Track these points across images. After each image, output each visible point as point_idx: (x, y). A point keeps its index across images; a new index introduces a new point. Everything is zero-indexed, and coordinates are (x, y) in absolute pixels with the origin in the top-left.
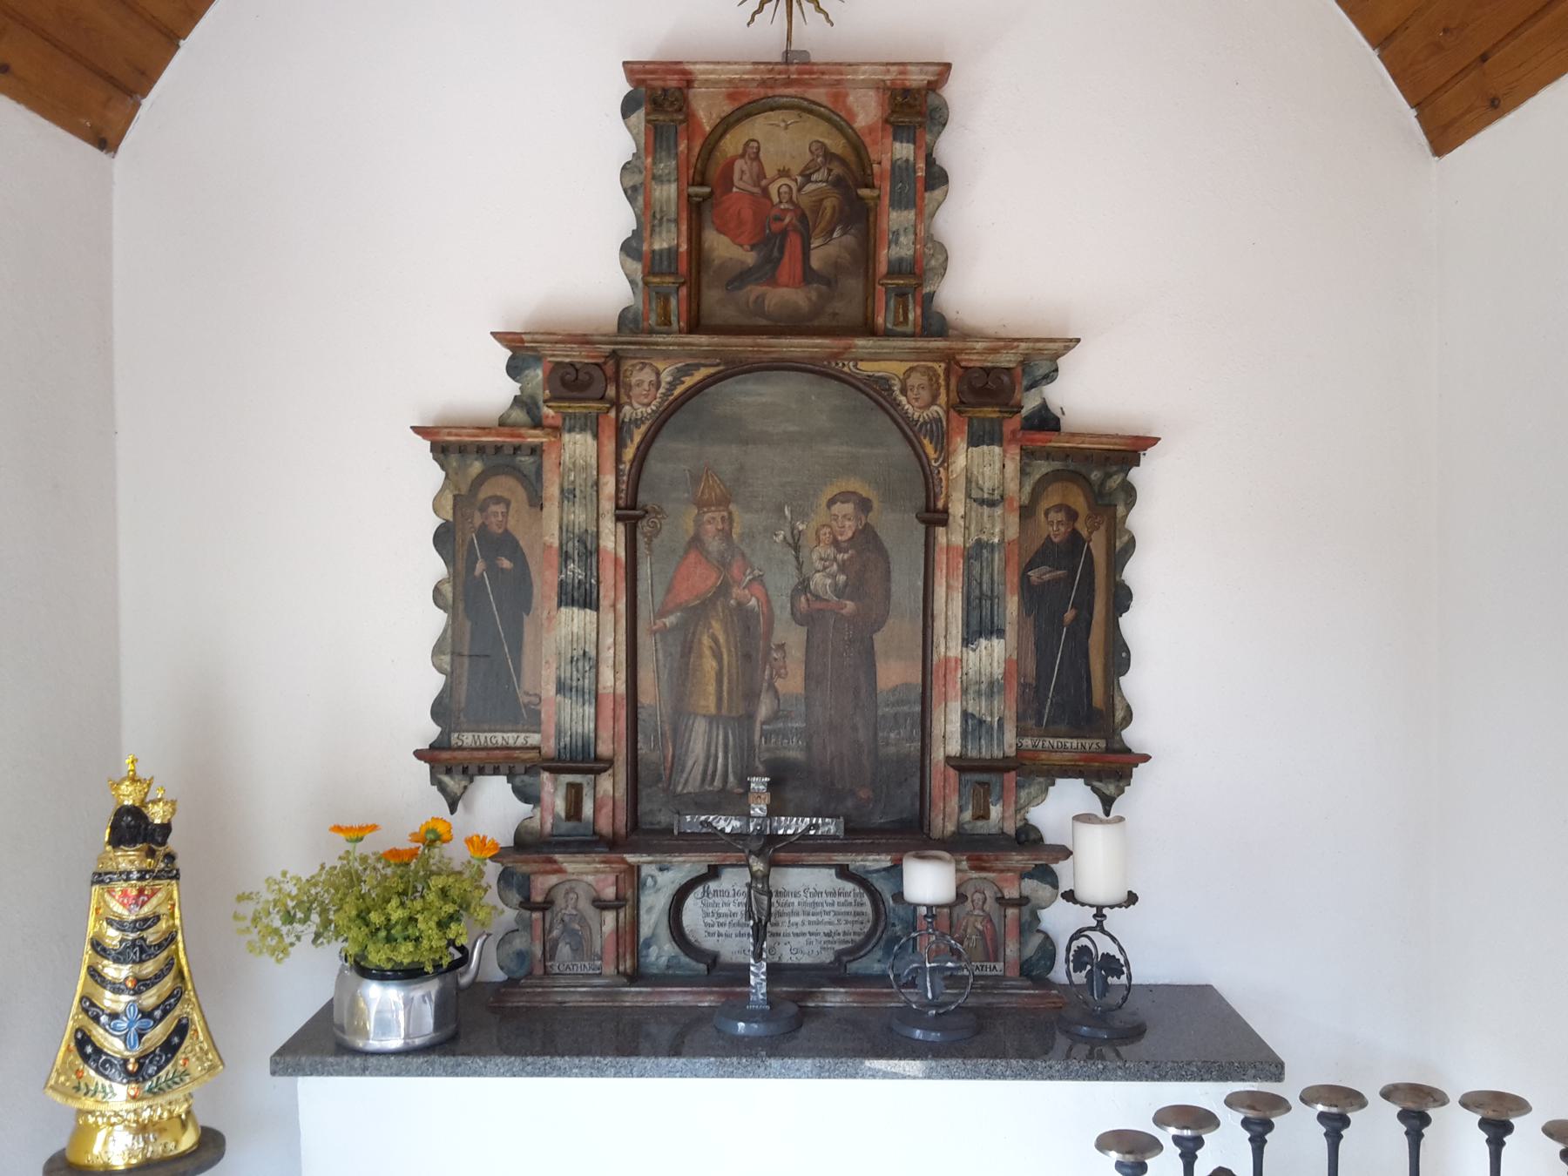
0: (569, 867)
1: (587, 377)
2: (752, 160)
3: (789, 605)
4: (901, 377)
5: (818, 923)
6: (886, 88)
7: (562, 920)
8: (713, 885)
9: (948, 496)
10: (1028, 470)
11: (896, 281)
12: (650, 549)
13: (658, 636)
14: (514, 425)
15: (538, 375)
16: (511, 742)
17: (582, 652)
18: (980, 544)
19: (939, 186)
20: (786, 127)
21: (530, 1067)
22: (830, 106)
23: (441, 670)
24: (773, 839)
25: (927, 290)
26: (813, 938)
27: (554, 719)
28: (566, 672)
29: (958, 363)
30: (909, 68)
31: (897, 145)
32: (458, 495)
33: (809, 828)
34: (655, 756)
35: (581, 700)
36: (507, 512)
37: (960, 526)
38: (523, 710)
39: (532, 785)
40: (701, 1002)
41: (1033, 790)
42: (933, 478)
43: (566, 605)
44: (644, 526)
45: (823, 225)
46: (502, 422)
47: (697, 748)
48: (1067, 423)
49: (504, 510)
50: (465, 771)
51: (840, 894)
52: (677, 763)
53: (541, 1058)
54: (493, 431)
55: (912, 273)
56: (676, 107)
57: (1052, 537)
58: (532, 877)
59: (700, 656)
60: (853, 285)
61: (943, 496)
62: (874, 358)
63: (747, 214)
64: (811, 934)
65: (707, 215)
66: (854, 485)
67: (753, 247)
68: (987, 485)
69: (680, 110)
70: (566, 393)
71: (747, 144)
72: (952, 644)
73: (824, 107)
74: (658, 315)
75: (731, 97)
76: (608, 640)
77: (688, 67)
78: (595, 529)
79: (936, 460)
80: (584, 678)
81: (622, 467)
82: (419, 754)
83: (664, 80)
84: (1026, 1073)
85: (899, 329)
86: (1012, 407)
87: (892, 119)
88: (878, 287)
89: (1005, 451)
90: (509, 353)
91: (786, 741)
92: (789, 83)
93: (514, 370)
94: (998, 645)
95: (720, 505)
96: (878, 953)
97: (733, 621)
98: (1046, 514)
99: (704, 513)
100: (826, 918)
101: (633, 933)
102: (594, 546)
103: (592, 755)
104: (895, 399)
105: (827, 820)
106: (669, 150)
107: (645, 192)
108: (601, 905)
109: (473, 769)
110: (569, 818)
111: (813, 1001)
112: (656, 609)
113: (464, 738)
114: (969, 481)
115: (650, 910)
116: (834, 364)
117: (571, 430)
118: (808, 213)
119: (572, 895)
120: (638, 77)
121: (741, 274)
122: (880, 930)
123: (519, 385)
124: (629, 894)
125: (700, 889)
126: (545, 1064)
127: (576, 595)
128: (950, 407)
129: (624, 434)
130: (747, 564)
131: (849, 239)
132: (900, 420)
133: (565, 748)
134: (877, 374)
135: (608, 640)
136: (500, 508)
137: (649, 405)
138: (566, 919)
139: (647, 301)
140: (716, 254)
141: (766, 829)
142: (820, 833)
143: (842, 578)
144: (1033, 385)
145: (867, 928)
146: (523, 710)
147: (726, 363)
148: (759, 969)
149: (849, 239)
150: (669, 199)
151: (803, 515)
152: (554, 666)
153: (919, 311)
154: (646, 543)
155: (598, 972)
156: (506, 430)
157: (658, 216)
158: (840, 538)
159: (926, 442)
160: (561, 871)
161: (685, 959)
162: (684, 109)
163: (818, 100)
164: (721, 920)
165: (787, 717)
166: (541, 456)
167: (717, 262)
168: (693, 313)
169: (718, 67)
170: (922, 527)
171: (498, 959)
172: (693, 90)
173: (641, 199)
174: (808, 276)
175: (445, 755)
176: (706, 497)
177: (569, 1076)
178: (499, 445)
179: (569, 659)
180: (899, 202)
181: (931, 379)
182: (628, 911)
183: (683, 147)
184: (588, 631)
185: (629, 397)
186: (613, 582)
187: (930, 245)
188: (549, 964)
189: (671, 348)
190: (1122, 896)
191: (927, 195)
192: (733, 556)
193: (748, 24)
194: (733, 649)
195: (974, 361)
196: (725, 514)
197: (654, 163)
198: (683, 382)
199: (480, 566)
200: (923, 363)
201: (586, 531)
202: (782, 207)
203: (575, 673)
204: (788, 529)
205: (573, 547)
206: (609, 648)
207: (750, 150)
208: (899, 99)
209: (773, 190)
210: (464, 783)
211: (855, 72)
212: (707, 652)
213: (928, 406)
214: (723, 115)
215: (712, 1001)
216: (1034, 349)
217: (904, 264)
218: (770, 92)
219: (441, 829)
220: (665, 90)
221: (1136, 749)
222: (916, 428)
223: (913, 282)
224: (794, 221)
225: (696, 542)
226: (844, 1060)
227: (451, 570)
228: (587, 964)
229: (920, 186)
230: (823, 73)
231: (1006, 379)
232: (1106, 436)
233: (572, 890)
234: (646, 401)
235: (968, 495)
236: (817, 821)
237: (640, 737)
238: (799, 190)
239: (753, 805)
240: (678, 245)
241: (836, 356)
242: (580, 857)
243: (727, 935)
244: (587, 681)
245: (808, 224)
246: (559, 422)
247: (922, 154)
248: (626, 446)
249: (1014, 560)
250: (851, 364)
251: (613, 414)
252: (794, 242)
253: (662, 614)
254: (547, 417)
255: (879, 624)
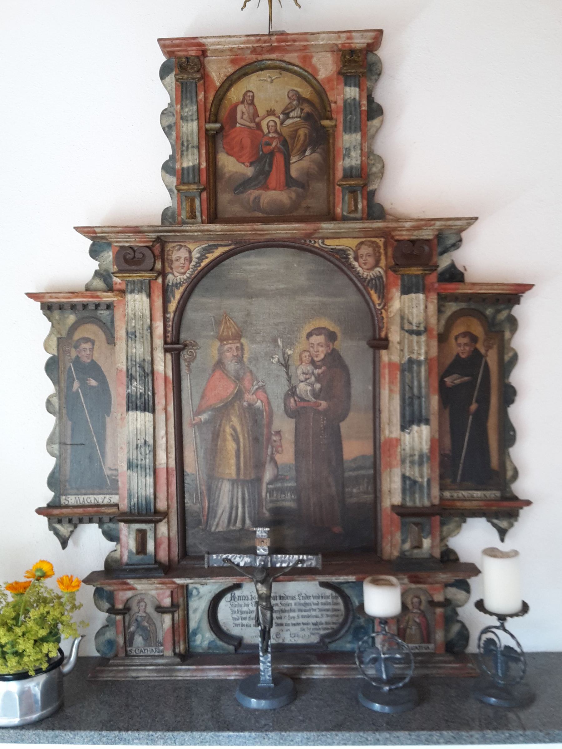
0: (139, 587)
1: (141, 256)
2: (249, 104)
3: (283, 404)
4: (354, 249)
5: (308, 617)
6: (340, 50)
7: (137, 620)
8: (237, 593)
9: (388, 329)
10: (443, 309)
11: (349, 183)
12: (190, 370)
13: (196, 427)
14: (96, 290)
15: (109, 255)
16: (100, 502)
17: (143, 441)
18: (411, 361)
19: (377, 117)
20: (272, 81)
21: (104, 739)
22: (300, 65)
23: (53, 455)
24: (274, 570)
25: (371, 188)
26: (305, 627)
27: (127, 486)
28: (133, 454)
29: (392, 237)
30: (354, 34)
31: (348, 89)
32: (60, 338)
33: (297, 563)
34: (196, 507)
35: (143, 473)
36: (93, 349)
37: (396, 348)
38: (108, 479)
39: (114, 529)
40: (229, 676)
41: (452, 526)
42: (377, 317)
43: (132, 410)
44: (185, 355)
45: (299, 146)
46: (88, 288)
47: (224, 501)
48: (470, 277)
49: (91, 347)
50: (70, 521)
51: (322, 597)
52: (212, 511)
53: (112, 733)
54: (80, 294)
55: (360, 176)
56: (195, 69)
57: (461, 354)
58: (115, 593)
59: (225, 440)
60: (319, 187)
61: (384, 329)
62: (336, 236)
63: (247, 142)
64: (304, 624)
65: (220, 143)
66: (308, 329)
67: (251, 164)
68: (415, 321)
69: (198, 71)
70: (127, 267)
71: (245, 94)
72: (394, 429)
73: (297, 66)
74: (187, 212)
75: (233, 62)
76: (161, 432)
77: (201, 41)
78: (150, 358)
79: (379, 305)
80: (145, 458)
81: (168, 316)
82: (39, 511)
83: (187, 51)
84: (453, 740)
85: (352, 215)
86: (432, 266)
87: (343, 71)
88: (337, 187)
89: (427, 297)
90: (91, 242)
91: (284, 495)
92: (272, 50)
93: (94, 253)
94: (425, 430)
95: (235, 339)
96: (349, 638)
97: (245, 417)
98: (456, 338)
99: (225, 344)
100: (314, 613)
101: (184, 626)
102: (150, 369)
103: (153, 510)
104: (350, 264)
105: (310, 557)
106: (191, 99)
107: (177, 128)
108: (160, 610)
109: (75, 520)
110: (138, 553)
111: (305, 675)
112: (195, 410)
113: (69, 499)
114: (402, 318)
115: (195, 611)
116: (308, 242)
117: (132, 292)
118: (289, 140)
119: (142, 604)
120: (168, 49)
121: (244, 182)
122: (350, 620)
123: (98, 263)
124: (181, 601)
125: (228, 596)
126: (115, 737)
127: (139, 403)
128: (388, 268)
129: (169, 294)
130: (254, 378)
131: (316, 156)
132: (354, 278)
133: (134, 506)
134: (338, 248)
135: (161, 432)
136: (88, 346)
137: (184, 273)
138: (139, 619)
139: (180, 203)
140: (226, 170)
141: (268, 563)
142: (305, 565)
143: (318, 386)
144: (445, 251)
145: (341, 620)
146: (108, 479)
147: (235, 244)
148: (266, 659)
149: (316, 156)
150: (192, 132)
151: (290, 344)
152: (126, 451)
153: (365, 202)
154: (187, 366)
155: (161, 654)
156: (88, 293)
157: (185, 144)
158: (316, 359)
159: (372, 292)
160: (133, 589)
161: (220, 643)
162: (202, 71)
163: (292, 61)
164: (244, 616)
165: (283, 480)
166: (113, 310)
167: (227, 175)
168: (211, 210)
169: (222, 40)
170: (371, 351)
171: (96, 645)
172: (208, 58)
173: (174, 134)
174: (290, 182)
175: (56, 512)
176: (225, 334)
177: (132, 744)
178: (85, 304)
179: (135, 446)
180: (349, 128)
181: (374, 250)
182: (181, 613)
183: (201, 96)
184: (147, 427)
185: (172, 269)
186: (164, 393)
187: (371, 157)
188: (129, 649)
189: (196, 234)
190: (517, 606)
191: (369, 123)
192: (244, 373)
193: (242, 9)
194: (246, 435)
195: (405, 235)
196: (239, 345)
197: (182, 108)
198: (207, 258)
199: (76, 385)
200: (369, 239)
201: (144, 360)
202: (270, 136)
203: (139, 455)
204: (281, 354)
205: (136, 371)
206: (162, 438)
207: (247, 98)
208: (348, 57)
209: (264, 124)
210: (71, 529)
211: (317, 39)
212: (229, 438)
213: (372, 268)
214: (228, 74)
215: (236, 676)
216: (445, 226)
217: (354, 170)
218: (260, 58)
219: (45, 568)
220: (187, 58)
221: (522, 496)
222: (365, 284)
223: (360, 182)
224: (279, 145)
225: (220, 364)
226: (324, 733)
227: (58, 388)
228: (154, 649)
229: (364, 117)
230: (295, 41)
231: (427, 248)
232: (497, 284)
233: (142, 600)
234: (183, 271)
235: (402, 328)
236: (303, 557)
237: (186, 495)
238: (282, 123)
239: (258, 547)
240: (200, 164)
241: (309, 236)
242: (144, 581)
243: (247, 626)
244: (147, 461)
245: (288, 147)
246: (123, 287)
247: (365, 95)
248: (170, 302)
249: (435, 370)
250: (320, 241)
251: (160, 280)
252: (279, 159)
253: (199, 413)
254: (116, 284)
255: (343, 417)
